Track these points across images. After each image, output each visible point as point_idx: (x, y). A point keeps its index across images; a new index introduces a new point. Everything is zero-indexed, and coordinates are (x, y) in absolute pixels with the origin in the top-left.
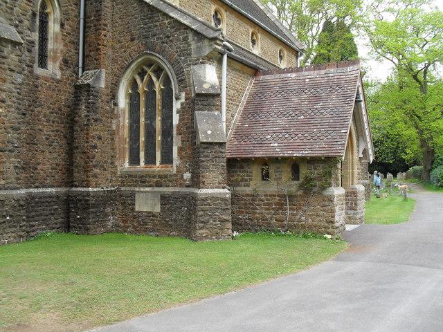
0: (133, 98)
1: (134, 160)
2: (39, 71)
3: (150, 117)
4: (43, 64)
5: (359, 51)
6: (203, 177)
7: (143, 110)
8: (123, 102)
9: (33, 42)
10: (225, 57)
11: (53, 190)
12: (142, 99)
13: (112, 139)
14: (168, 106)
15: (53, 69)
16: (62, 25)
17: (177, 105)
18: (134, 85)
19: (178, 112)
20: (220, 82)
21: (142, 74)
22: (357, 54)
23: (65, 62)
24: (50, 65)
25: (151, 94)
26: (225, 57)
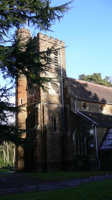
0: (76, 137)
1: (77, 152)
2: (54, 132)
3: (80, 142)
4: (55, 130)
5: (103, 110)
6: (38, 26)
7: (78, 140)
8: (74, 138)
9: (53, 126)
10: (95, 127)
11: (59, 160)
12: (78, 138)
13: (72, 147)
14: (83, 139)
15: (58, 131)
16: (59, 121)
17: (85, 139)
18: (76, 134)
19: (86, 141)
20: (95, 134)
21: (78, 132)
22: (102, 110)
23: (60, 129)
24: (57, 130)
25: (80, 136)
26: (95, 127)
